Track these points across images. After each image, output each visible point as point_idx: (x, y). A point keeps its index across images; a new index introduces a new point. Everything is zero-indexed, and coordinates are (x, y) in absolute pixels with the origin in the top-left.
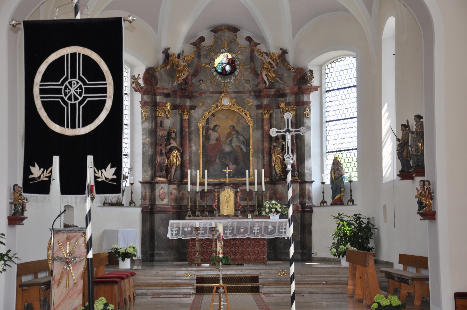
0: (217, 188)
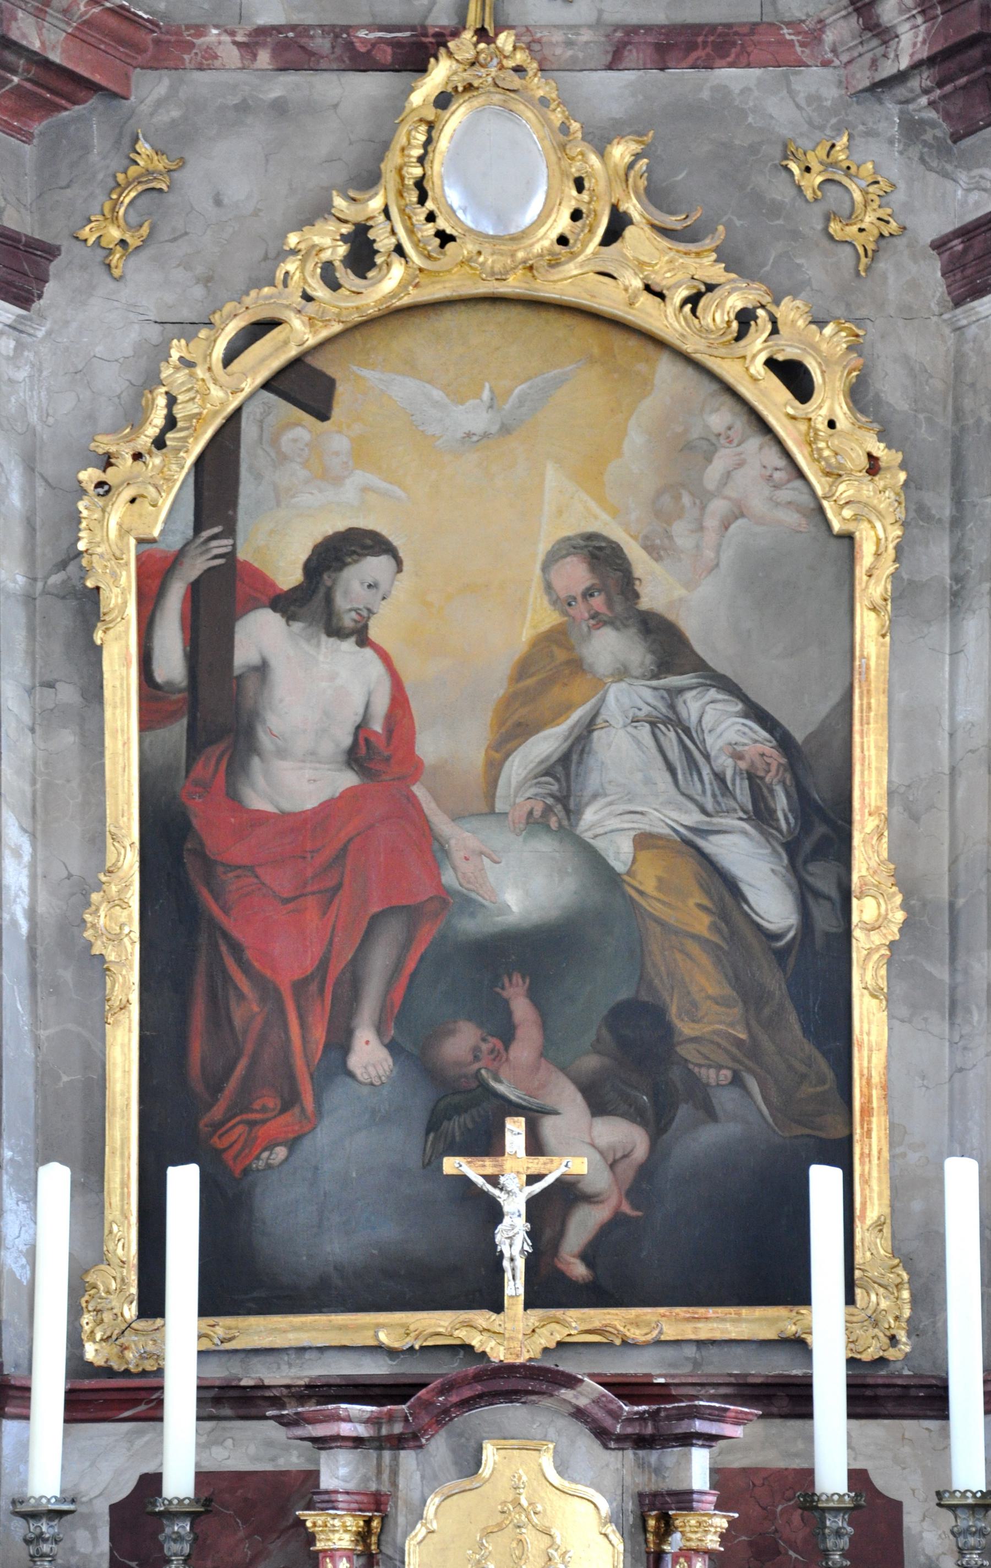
0: (357, 1442)
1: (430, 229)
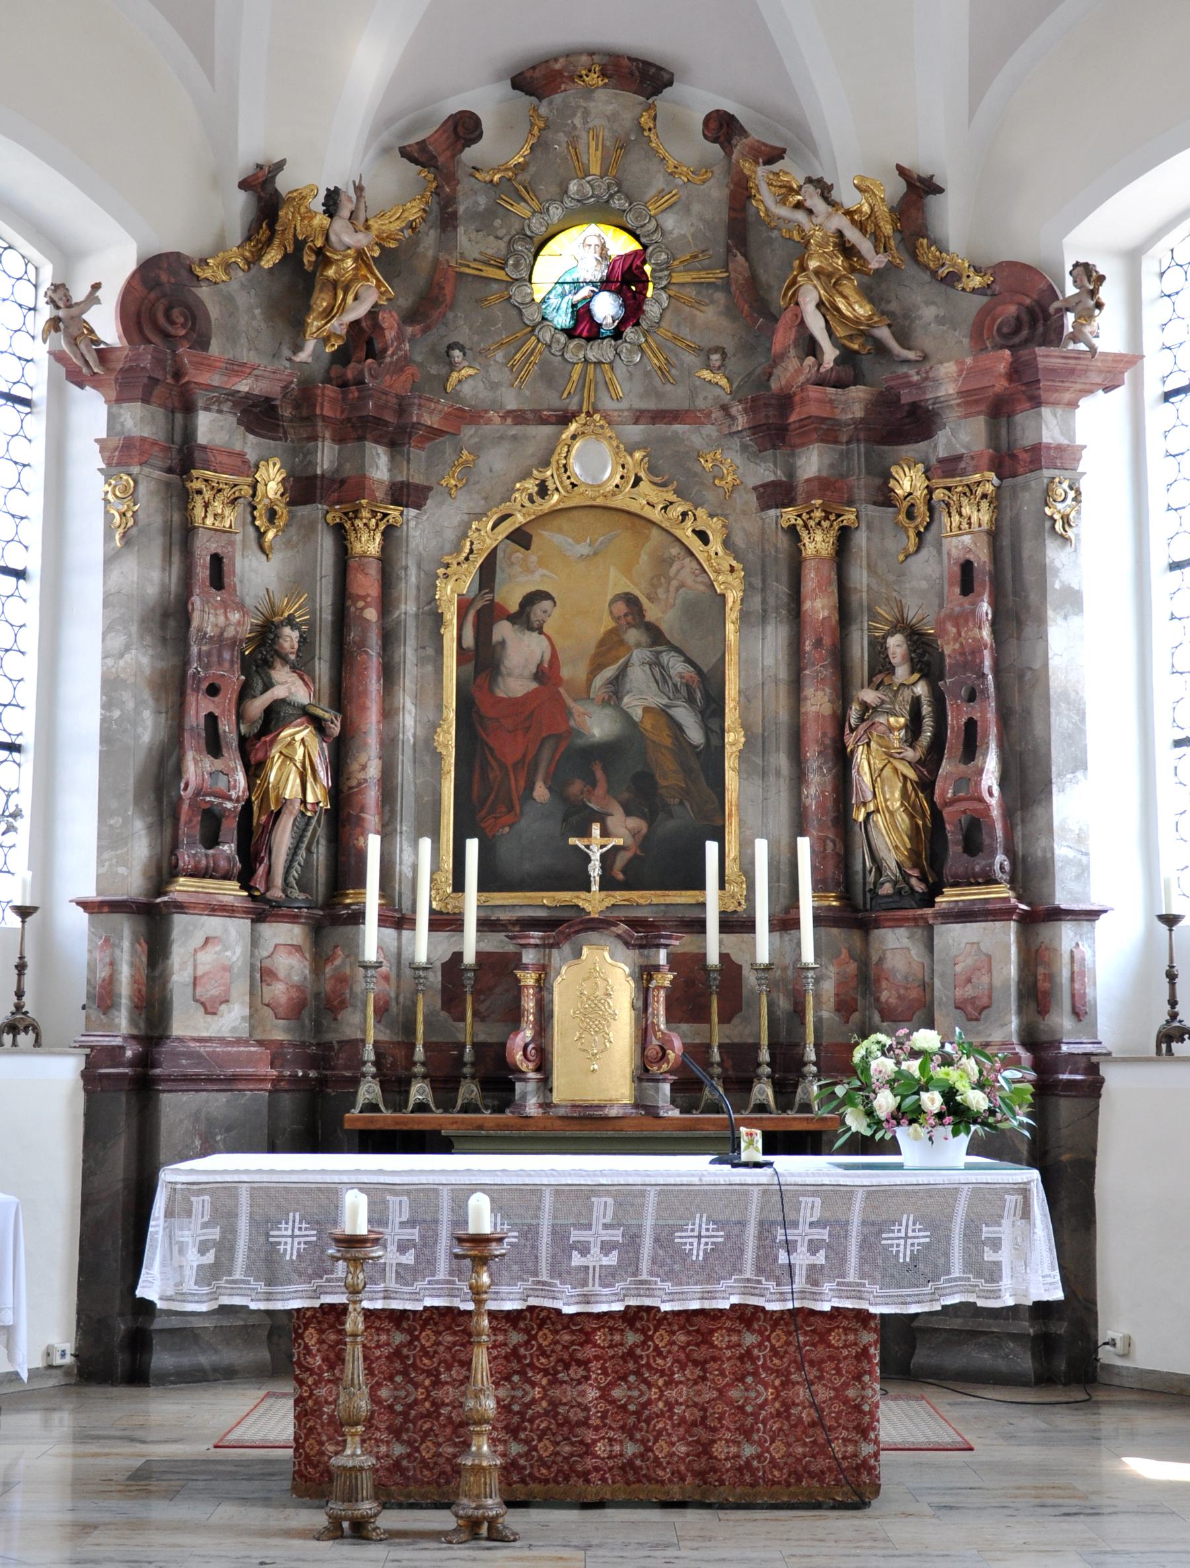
0: (536, 946)
1: (568, 482)
